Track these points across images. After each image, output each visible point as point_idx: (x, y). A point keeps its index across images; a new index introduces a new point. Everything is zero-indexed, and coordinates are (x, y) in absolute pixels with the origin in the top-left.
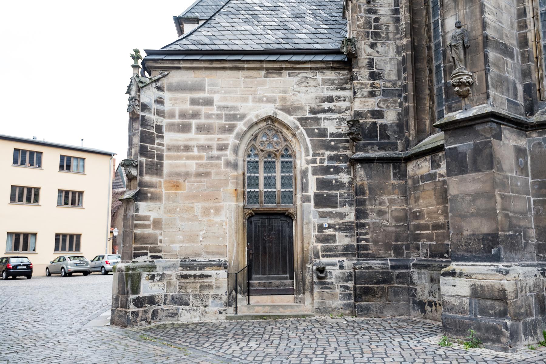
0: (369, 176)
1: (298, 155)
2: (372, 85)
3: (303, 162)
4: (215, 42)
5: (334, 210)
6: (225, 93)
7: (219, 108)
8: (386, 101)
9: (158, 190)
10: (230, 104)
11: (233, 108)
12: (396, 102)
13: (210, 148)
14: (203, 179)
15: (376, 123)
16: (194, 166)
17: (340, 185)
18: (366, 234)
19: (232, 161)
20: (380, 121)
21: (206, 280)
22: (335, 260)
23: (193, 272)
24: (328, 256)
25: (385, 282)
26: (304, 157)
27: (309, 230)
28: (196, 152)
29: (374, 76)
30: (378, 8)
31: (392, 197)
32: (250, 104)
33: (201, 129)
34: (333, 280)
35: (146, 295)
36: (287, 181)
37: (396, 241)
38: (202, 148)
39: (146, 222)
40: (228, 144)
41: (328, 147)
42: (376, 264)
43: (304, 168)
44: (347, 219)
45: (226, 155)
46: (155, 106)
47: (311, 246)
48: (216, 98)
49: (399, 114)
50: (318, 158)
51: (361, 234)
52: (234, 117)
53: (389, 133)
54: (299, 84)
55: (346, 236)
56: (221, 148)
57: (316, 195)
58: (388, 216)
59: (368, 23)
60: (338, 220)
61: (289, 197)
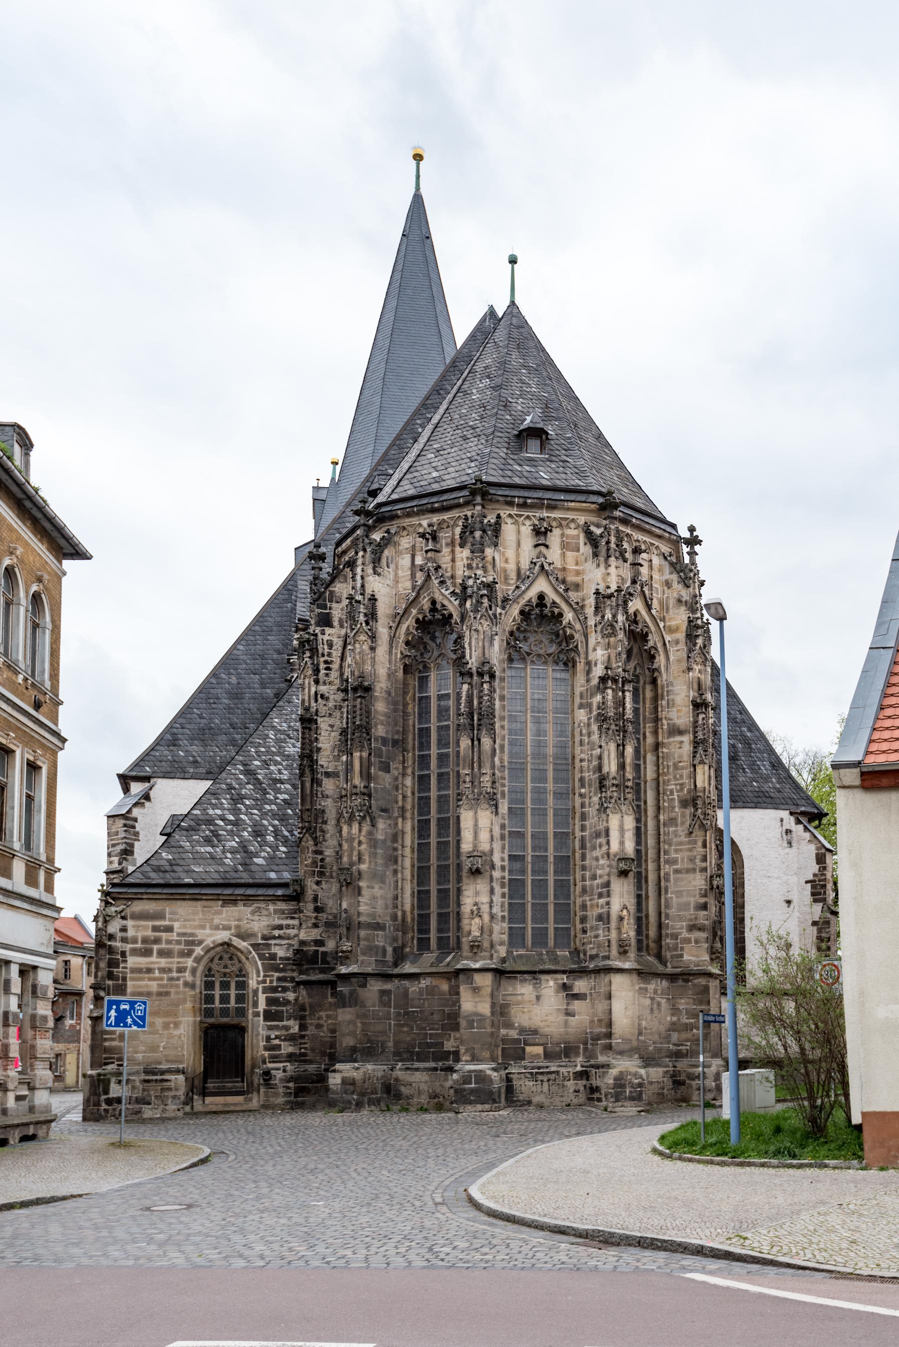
2: (316, 918)
3: (255, 982)
5: (281, 1024)
6: (185, 921)
7: (179, 934)
10: (189, 931)
11: (192, 935)
13: (170, 970)
16: (156, 986)
17: (287, 1002)
18: (305, 1043)
20: (321, 949)
22: (281, 1065)
23: (155, 1077)
24: (274, 1062)
25: (318, 1081)
27: (258, 1040)
28: (157, 974)
29: (317, 910)
32: (208, 931)
33: (162, 953)
34: (277, 1082)
35: (115, 1096)
36: (240, 999)
38: (162, 970)
39: (113, 1036)
41: (277, 969)
44: (292, 1031)
46: (119, 935)
48: (176, 925)
50: (268, 979)
51: (301, 1044)
52: (193, 943)
53: (329, 959)
54: (253, 913)
56: (181, 970)
58: (325, 1028)
59: (314, 863)
60: (284, 1032)
61: (241, 1012)
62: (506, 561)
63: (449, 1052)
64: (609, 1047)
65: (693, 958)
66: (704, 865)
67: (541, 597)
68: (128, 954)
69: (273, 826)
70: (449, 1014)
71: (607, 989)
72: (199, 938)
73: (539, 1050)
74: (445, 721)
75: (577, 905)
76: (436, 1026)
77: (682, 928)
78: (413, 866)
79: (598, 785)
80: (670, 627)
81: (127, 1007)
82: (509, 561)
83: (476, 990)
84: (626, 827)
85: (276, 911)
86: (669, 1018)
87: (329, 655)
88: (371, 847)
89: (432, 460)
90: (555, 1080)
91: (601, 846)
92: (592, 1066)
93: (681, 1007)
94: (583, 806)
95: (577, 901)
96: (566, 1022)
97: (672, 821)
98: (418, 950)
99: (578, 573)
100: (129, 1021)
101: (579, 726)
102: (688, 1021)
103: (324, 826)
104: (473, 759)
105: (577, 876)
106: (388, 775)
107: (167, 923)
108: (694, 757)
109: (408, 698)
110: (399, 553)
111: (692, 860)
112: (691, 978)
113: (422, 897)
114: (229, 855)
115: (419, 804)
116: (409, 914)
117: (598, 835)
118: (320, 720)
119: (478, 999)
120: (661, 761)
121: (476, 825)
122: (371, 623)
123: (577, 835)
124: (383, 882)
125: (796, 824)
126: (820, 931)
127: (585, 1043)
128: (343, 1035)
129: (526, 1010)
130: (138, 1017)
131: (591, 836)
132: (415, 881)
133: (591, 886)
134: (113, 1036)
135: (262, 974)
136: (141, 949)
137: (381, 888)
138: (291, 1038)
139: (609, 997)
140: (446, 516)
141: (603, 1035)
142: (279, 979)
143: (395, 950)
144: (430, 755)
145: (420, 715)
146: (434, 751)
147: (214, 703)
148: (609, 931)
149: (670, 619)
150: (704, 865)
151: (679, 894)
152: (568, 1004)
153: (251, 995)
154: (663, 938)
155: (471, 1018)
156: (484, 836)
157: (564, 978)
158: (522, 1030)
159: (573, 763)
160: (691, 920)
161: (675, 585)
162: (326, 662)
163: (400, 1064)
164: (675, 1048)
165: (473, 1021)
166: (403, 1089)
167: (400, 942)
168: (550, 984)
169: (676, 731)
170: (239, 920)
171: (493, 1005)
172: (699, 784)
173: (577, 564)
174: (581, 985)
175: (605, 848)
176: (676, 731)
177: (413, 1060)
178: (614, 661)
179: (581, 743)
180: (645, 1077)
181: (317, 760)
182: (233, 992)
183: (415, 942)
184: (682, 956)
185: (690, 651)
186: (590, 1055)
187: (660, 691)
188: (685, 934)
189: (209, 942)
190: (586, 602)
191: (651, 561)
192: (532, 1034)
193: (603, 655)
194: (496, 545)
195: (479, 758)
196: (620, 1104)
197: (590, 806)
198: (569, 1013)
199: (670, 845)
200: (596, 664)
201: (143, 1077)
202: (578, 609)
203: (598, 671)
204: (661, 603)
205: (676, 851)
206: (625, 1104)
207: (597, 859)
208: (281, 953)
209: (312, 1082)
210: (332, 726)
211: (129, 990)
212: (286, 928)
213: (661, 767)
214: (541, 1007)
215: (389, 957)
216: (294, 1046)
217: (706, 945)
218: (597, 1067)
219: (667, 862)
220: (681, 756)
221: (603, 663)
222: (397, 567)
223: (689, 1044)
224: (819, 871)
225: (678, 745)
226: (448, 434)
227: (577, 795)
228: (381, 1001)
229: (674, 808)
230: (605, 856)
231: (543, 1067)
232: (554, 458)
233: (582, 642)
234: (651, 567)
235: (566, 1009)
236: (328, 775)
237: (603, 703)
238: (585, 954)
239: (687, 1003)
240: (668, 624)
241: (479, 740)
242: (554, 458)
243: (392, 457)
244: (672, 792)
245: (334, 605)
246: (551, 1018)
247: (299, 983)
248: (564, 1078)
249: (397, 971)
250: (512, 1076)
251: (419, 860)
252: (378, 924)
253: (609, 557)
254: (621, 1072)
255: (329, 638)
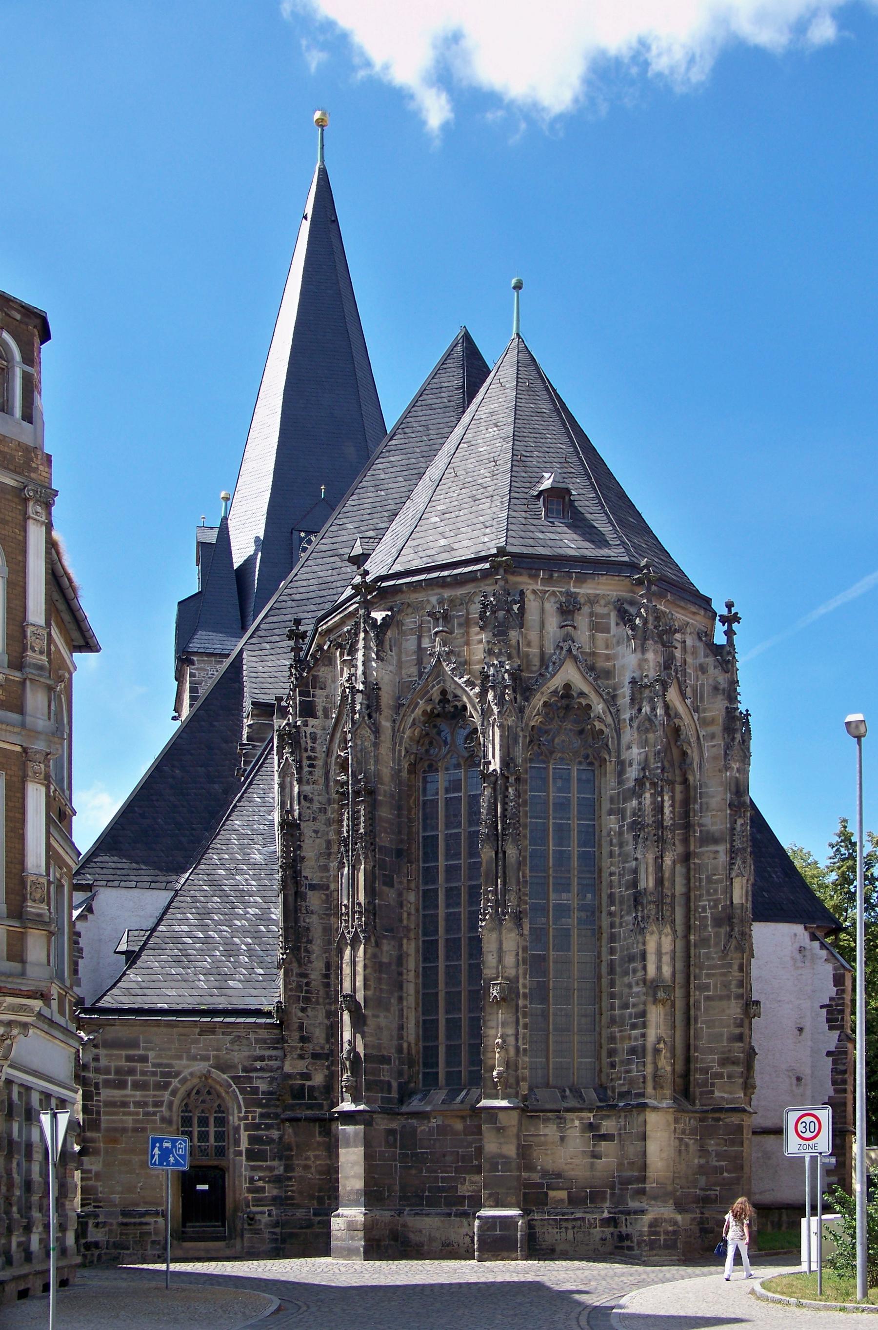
0: (296, 1134)
1: (230, 1111)
2: (302, 1048)
3: (236, 1119)
4: (147, 991)
5: (264, 1164)
6: (160, 1050)
7: (154, 1065)
8: (314, 1064)
9: (97, 1144)
10: (165, 1061)
11: (169, 1066)
12: (323, 1065)
13: (146, 1104)
14: (140, 1134)
15: (304, 1085)
16: (131, 1122)
17: (270, 1141)
18: (292, 1186)
19: (168, 1117)
20: (308, 1083)
21: (144, 1227)
22: (266, 1209)
23: (133, 1220)
24: (258, 1206)
25: (307, 1227)
26: (238, 1116)
27: (240, 1182)
28: (132, 1109)
29: (303, 1039)
30: (309, 972)
31: (317, 1153)
32: (184, 1062)
33: (136, 1086)
34: (262, 1227)
35: (93, 1240)
36: (220, 1136)
37: (319, 1192)
38: (137, 1104)
39: (90, 1175)
40: (163, 1101)
41: (260, 1105)
42: (300, 1213)
43: (236, 1124)
44: (276, 1172)
45: (162, 1111)
46: (93, 1064)
47: (243, 1196)
48: (151, 1054)
49: (326, 1076)
50: (250, 1115)
51: (288, 1186)
52: (168, 1075)
53: (316, 1094)
54: (232, 1042)
55: (275, 1188)
56: (157, 1104)
57: (247, 1149)
58: (313, 1170)
59: (299, 987)
60: (267, 1174)
61: (221, 1152)
62: (529, 645)
63: (464, 1197)
64: (642, 1192)
65: (725, 1095)
66: (740, 991)
67: (568, 686)
68: (101, 1085)
69: (246, 944)
70: (463, 1156)
71: (641, 1129)
72: (176, 1069)
73: (563, 1195)
74: (454, 828)
75: (603, 1036)
76: (449, 1169)
77: (713, 1061)
78: (417, 992)
79: (632, 902)
80: (704, 718)
81: (169, 1145)
82: (532, 644)
83: (501, 1130)
84: (664, 951)
85: (257, 1041)
86: (696, 1161)
87: (313, 749)
88: (375, 971)
89: (438, 525)
90: (580, 1227)
91: (635, 971)
92: (621, 1212)
93: (710, 1149)
94: (612, 925)
95: (604, 1032)
96: (592, 1164)
97: (704, 942)
98: (424, 1085)
99: (608, 658)
100: (172, 1159)
101: (609, 834)
102: (717, 1164)
103: (309, 946)
104: (497, 873)
105: (604, 1004)
106: (392, 891)
107: (141, 1052)
108: (731, 869)
109: (411, 801)
110: (402, 633)
111: (726, 985)
112: (722, 1116)
113: (428, 1029)
114: (202, 977)
115: (424, 923)
116: (413, 1045)
117: (631, 959)
118: (303, 825)
119: (502, 1140)
120: (692, 873)
121: (500, 949)
122: (374, 715)
123: (604, 959)
124: (388, 1010)
125: (812, 940)
126: (834, 1062)
127: (613, 1188)
128: (347, 1178)
129: (549, 1152)
130: (179, 1155)
131: (622, 959)
132: (420, 1009)
133: (622, 1017)
134: (90, 1175)
135: (243, 1110)
136: (114, 1080)
137: (386, 1017)
138: (277, 1180)
139: (644, 1137)
140: (460, 592)
141: (633, 1179)
142: (262, 1115)
143: (400, 1085)
144: (437, 868)
145: (425, 819)
146: (442, 863)
147: (157, 800)
148: (644, 1066)
149: (704, 711)
150: (740, 991)
151: (710, 1024)
152: (594, 1146)
153: (231, 1133)
154: (692, 1073)
155: (495, 1160)
156: (510, 960)
157: (590, 1116)
158: (545, 1174)
159: (600, 877)
160: (723, 1053)
161: (711, 670)
162: (309, 758)
163: (407, 1209)
164: (702, 1193)
165: (497, 1163)
166: (411, 1236)
167: (406, 1077)
168: (575, 1122)
169: (709, 839)
170: (217, 1050)
171: (519, 1147)
172: (736, 900)
173: (607, 648)
174: (608, 1126)
175: (640, 974)
176: (709, 839)
177: (422, 1205)
178: (652, 761)
179: (611, 855)
180: (680, 1223)
181: (300, 871)
182: (212, 1130)
183: (420, 1076)
184: (712, 1092)
185: (728, 747)
186: (618, 1200)
187: (692, 793)
188: (716, 1069)
189: (185, 1073)
190: (619, 692)
191: (685, 642)
192: (555, 1178)
193: (640, 754)
194: (522, 626)
195: (504, 873)
196: (655, 1252)
197: (621, 926)
198: (595, 1156)
199: (701, 969)
200: (631, 765)
201: (120, 1219)
202: (611, 700)
203: (632, 773)
204: (694, 691)
205: (708, 976)
206: (660, 1252)
207: (630, 986)
208: (263, 1086)
209: (302, 1228)
210: (316, 832)
211: (103, 1125)
212: (269, 1060)
213: (692, 881)
214: (567, 1150)
215: (394, 1095)
216: (279, 1188)
217: (741, 1080)
218: (628, 1213)
219: (698, 988)
220: (715, 868)
221: (639, 764)
222: (400, 651)
223: (718, 1188)
224: (837, 994)
225: (712, 856)
226: (452, 493)
227: (604, 914)
228: (387, 1142)
229: (706, 926)
230: (641, 982)
231: (567, 1214)
232: (579, 524)
233: (612, 738)
234: (684, 649)
235: (593, 1151)
236: (313, 887)
237: (640, 810)
238: (613, 1091)
239: (718, 1145)
240: (702, 715)
241: (504, 852)
242: (579, 524)
243: (351, 508)
244: (704, 909)
245: (318, 692)
246: (577, 1161)
247: (284, 1121)
248: (590, 1224)
249: (404, 1109)
250: (534, 1222)
251: (425, 986)
252: (383, 1056)
253: (645, 639)
254: (656, 1220)
255: (313, 730)
